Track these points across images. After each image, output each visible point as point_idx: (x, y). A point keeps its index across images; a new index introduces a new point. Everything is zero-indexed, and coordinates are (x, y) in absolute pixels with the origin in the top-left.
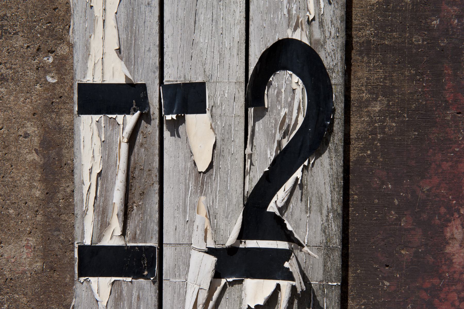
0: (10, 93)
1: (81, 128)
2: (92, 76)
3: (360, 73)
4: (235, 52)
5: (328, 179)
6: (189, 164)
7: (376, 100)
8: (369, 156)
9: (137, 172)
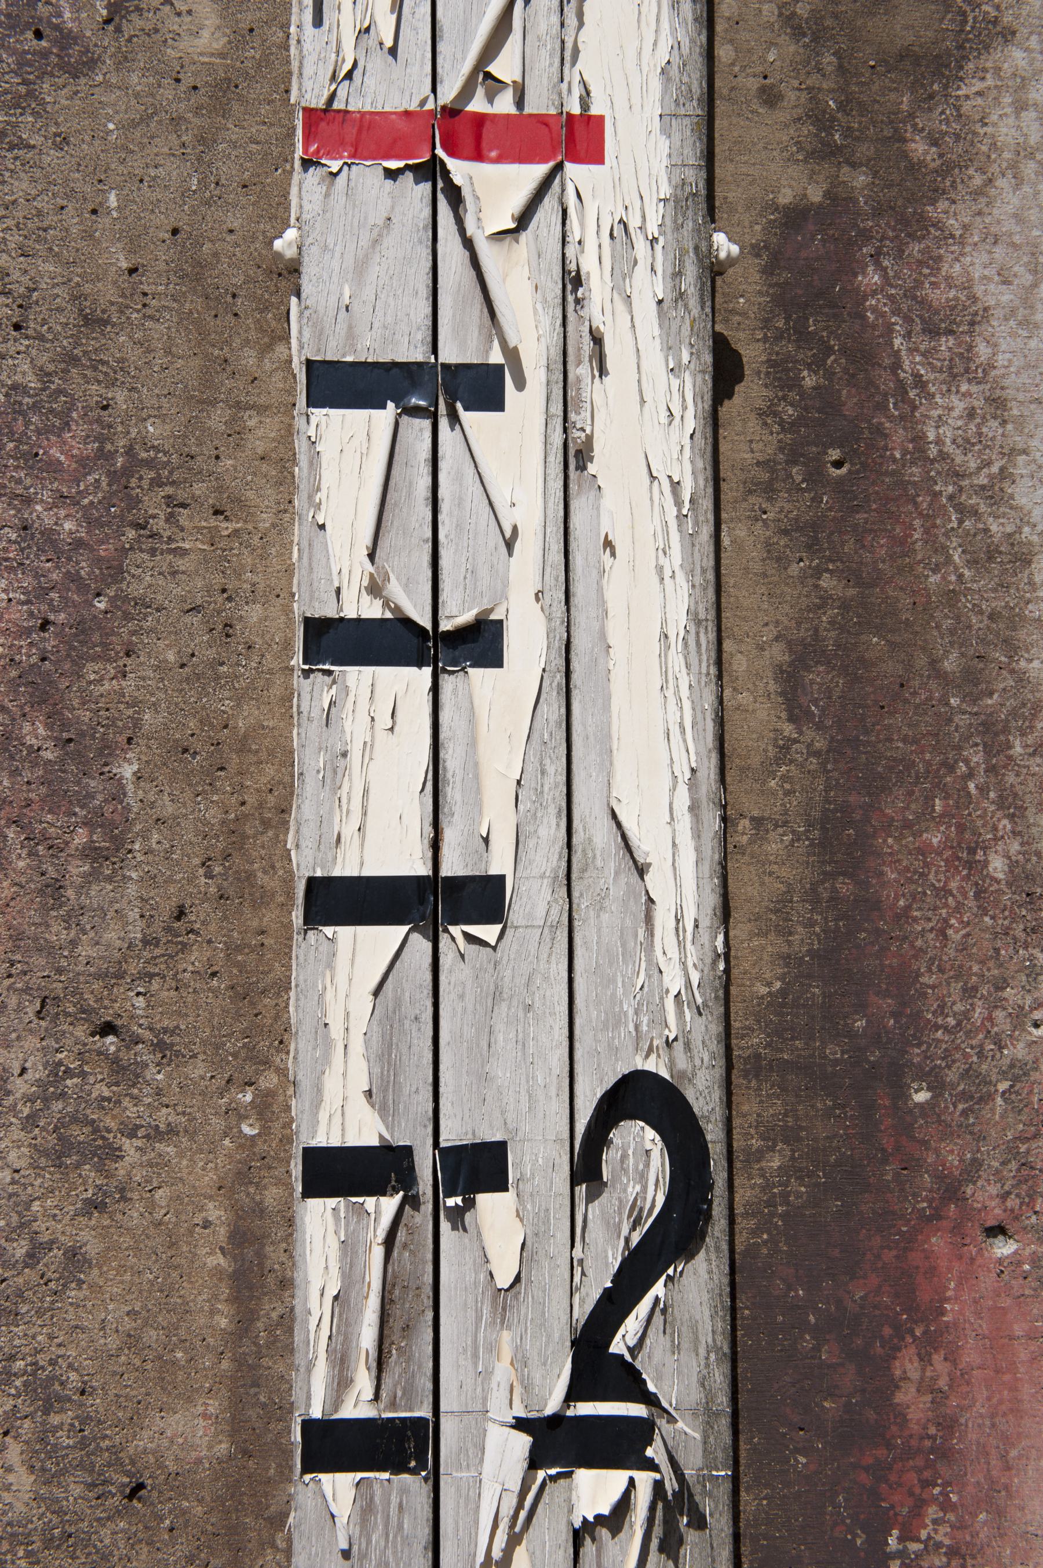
0: (181, 1155)
1: (307, 1219)
2: (327, 1136)
3: (747, 1106)
4: (553, 1091)
5: (706, 1297)
6: (482, 1277)
7: (772, 1149)
8: (765, 1242)
9: (397, 1292)
